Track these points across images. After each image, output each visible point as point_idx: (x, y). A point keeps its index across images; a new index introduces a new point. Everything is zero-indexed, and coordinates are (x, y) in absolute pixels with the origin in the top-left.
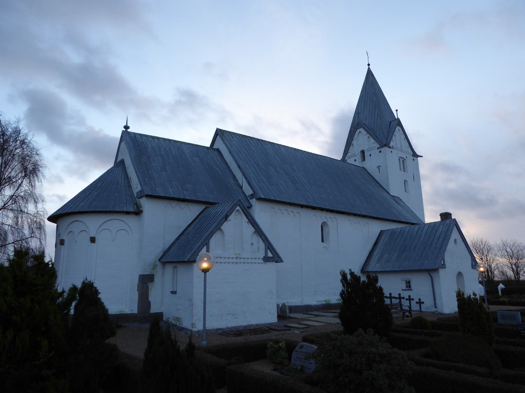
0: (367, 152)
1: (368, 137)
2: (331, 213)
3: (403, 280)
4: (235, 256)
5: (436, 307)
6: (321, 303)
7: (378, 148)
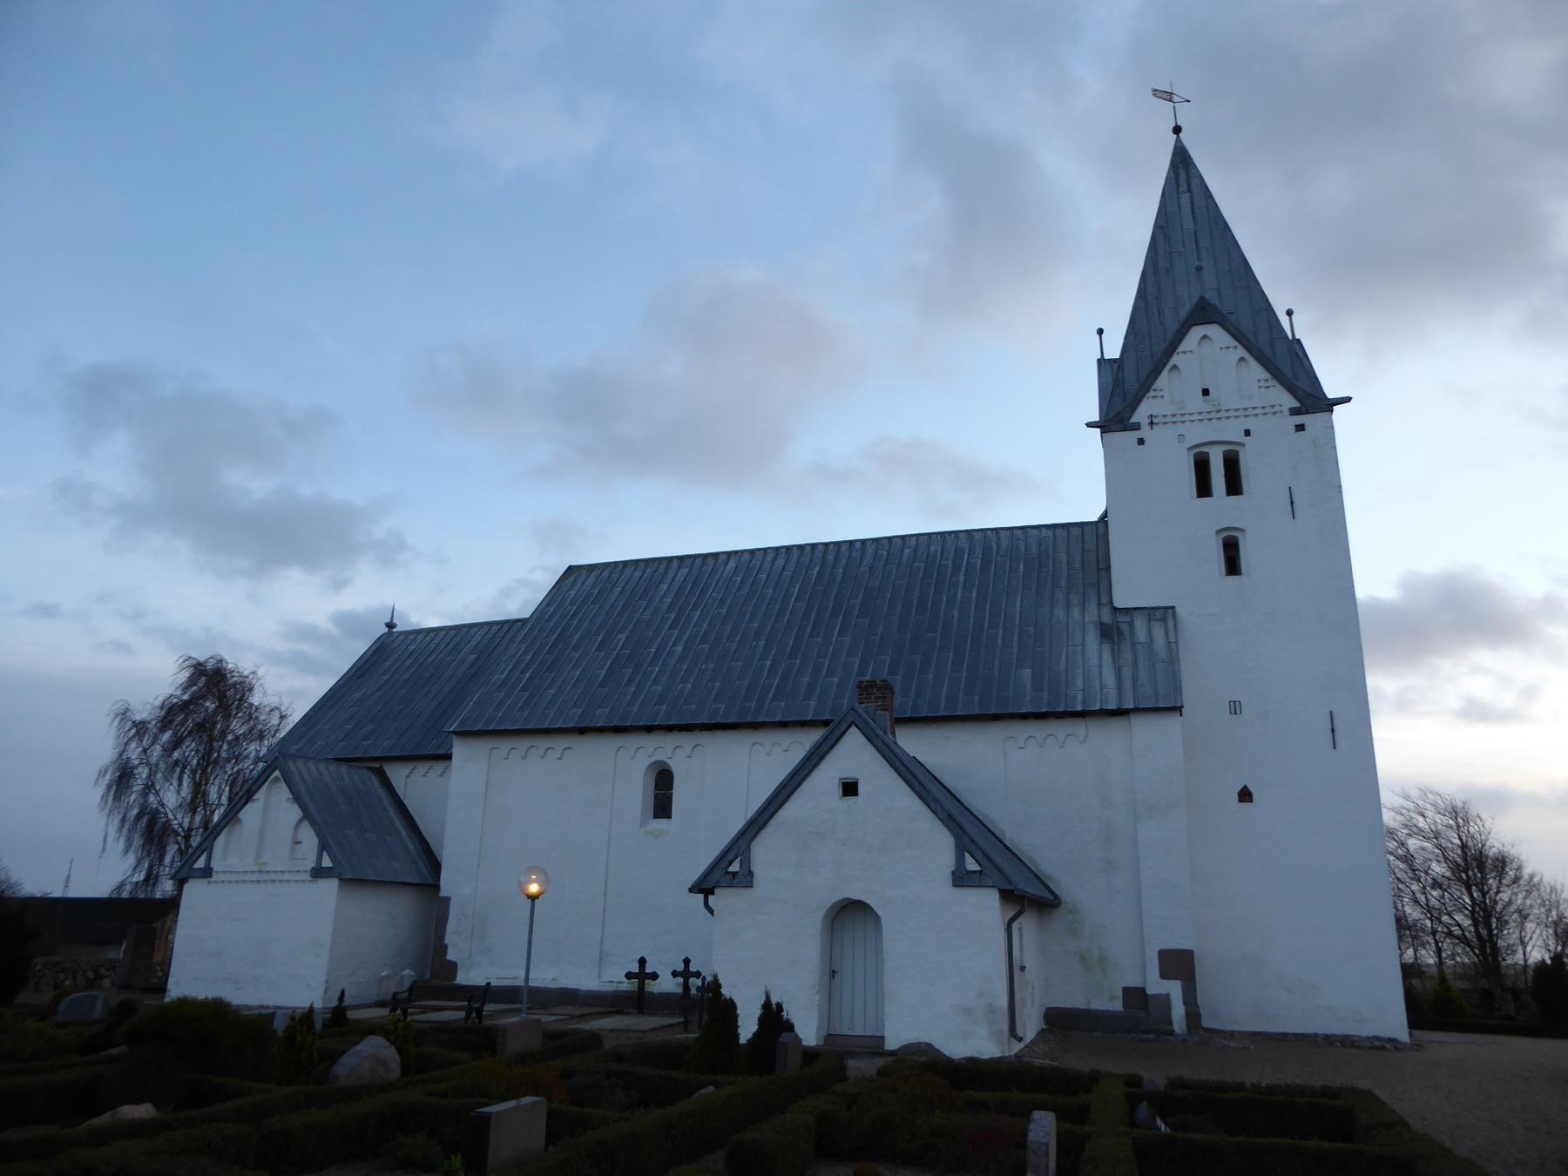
1: (1239, 357)
4: (255, 869)
6: (615, 989)
7: (1294, 412)
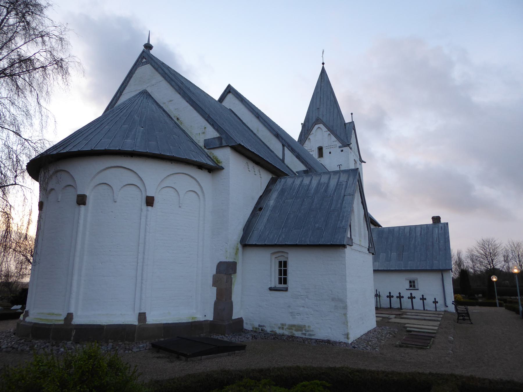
0: (326, 149)
3: (406, 280)
7: (340, 147)
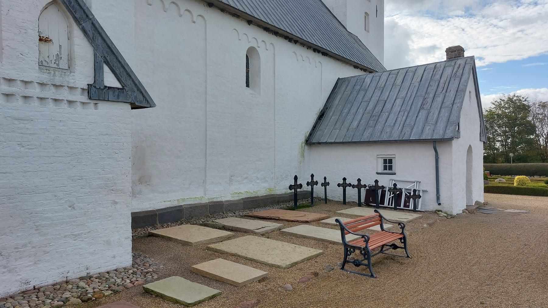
2: (265, 32)
5: (439, 204)
